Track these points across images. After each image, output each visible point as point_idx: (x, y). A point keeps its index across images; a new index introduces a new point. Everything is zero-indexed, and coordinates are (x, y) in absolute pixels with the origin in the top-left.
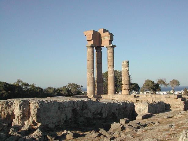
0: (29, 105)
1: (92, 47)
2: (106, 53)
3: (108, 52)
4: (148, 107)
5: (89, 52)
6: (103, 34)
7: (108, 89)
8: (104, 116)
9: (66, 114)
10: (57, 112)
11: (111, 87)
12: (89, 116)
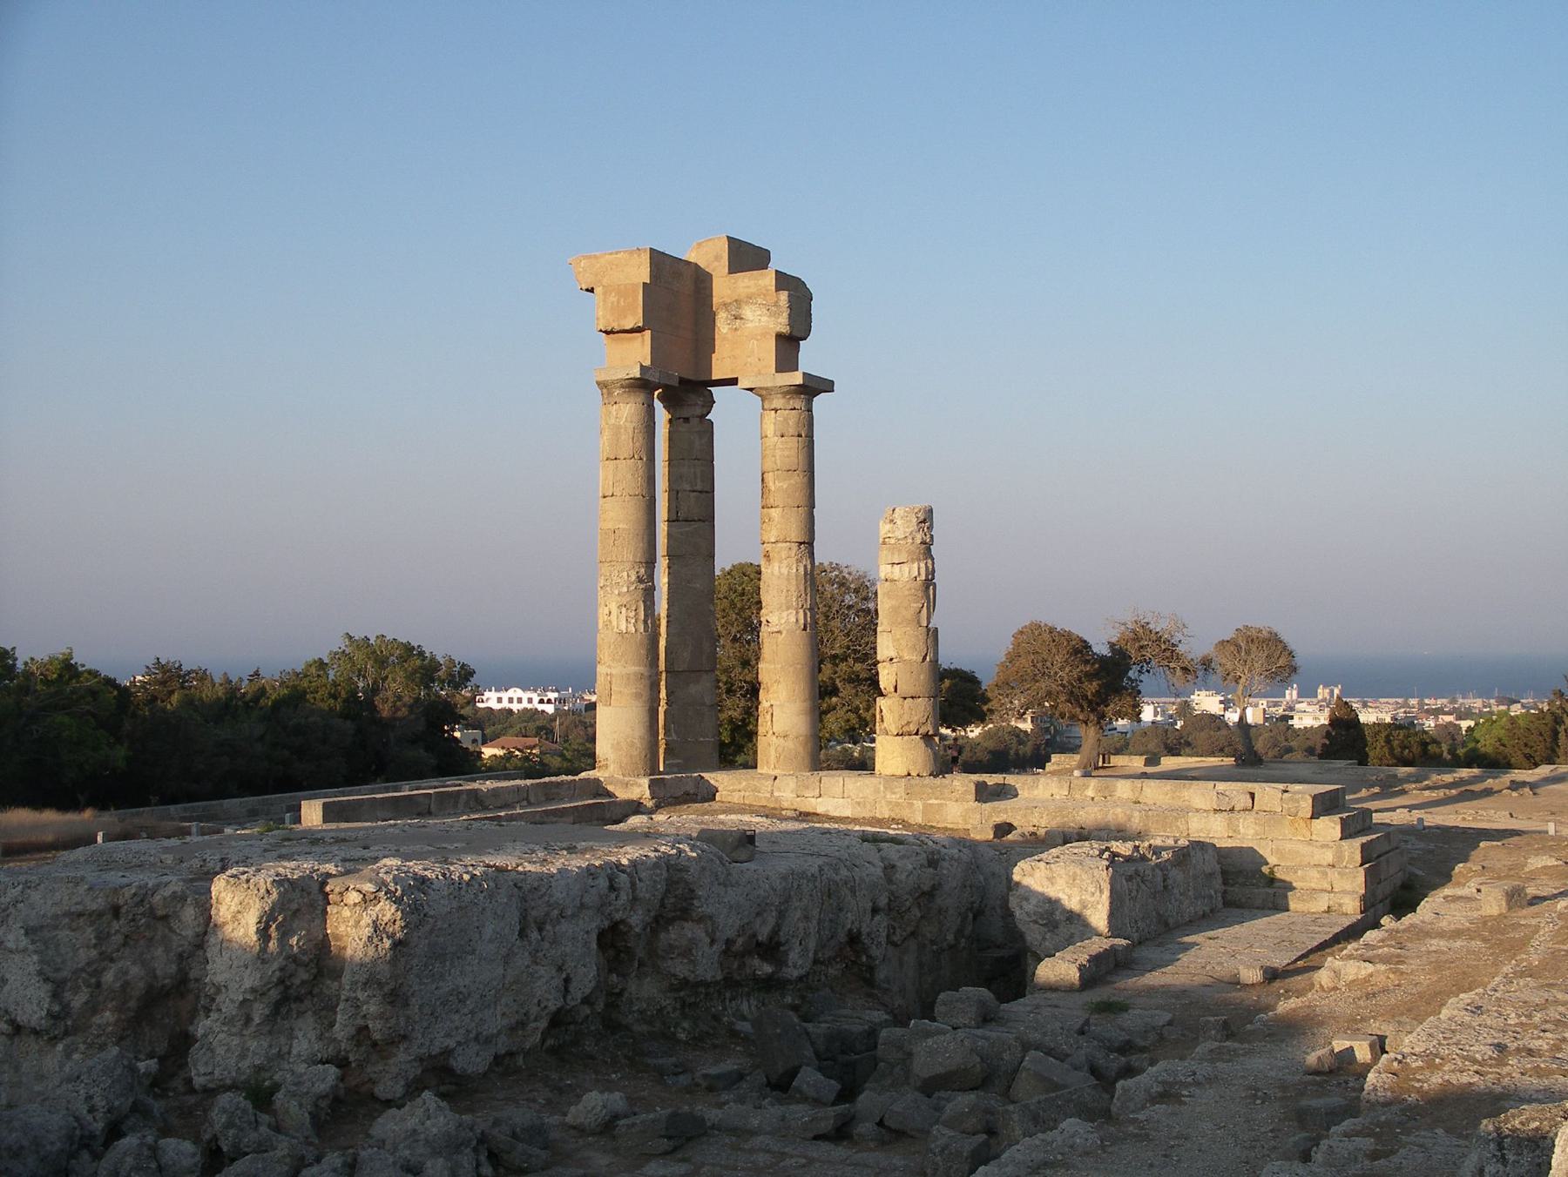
0: (325, 912)
1: (642, 385)
2: (744, 430)
3: (770, 429)
4: (1107, 894)
5: (617, 430)
6: (725, 287)
8: (797, 963)
9: (560, 969)
10: (507, 960)
11: (782, 711)
12: (700, 971)
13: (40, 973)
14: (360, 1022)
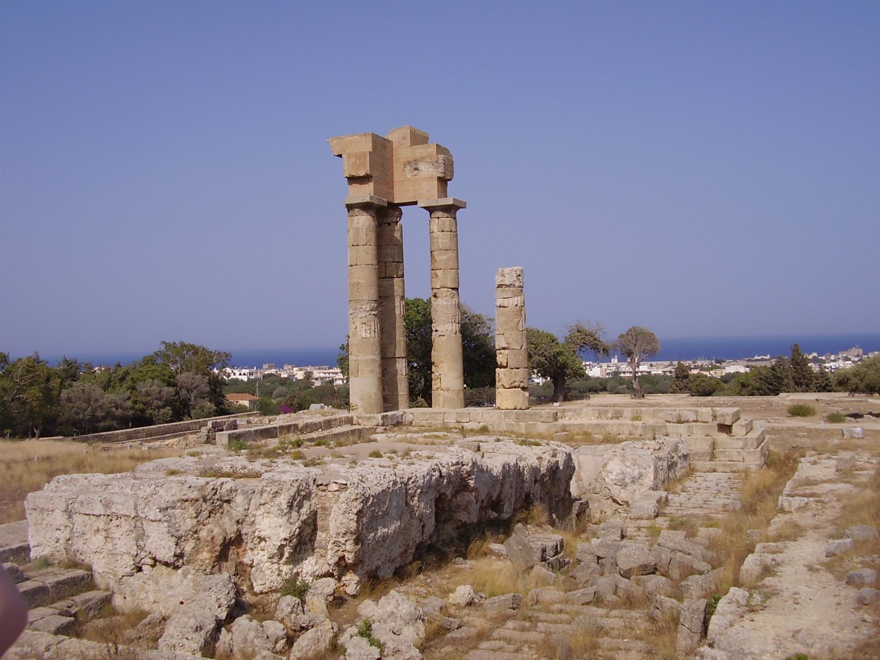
5: (357, 230)
7: (434, 387)
9: (421, 520)
13: (169, 532)
14: (340, 553)
